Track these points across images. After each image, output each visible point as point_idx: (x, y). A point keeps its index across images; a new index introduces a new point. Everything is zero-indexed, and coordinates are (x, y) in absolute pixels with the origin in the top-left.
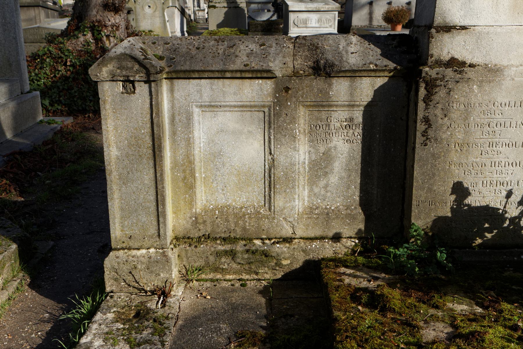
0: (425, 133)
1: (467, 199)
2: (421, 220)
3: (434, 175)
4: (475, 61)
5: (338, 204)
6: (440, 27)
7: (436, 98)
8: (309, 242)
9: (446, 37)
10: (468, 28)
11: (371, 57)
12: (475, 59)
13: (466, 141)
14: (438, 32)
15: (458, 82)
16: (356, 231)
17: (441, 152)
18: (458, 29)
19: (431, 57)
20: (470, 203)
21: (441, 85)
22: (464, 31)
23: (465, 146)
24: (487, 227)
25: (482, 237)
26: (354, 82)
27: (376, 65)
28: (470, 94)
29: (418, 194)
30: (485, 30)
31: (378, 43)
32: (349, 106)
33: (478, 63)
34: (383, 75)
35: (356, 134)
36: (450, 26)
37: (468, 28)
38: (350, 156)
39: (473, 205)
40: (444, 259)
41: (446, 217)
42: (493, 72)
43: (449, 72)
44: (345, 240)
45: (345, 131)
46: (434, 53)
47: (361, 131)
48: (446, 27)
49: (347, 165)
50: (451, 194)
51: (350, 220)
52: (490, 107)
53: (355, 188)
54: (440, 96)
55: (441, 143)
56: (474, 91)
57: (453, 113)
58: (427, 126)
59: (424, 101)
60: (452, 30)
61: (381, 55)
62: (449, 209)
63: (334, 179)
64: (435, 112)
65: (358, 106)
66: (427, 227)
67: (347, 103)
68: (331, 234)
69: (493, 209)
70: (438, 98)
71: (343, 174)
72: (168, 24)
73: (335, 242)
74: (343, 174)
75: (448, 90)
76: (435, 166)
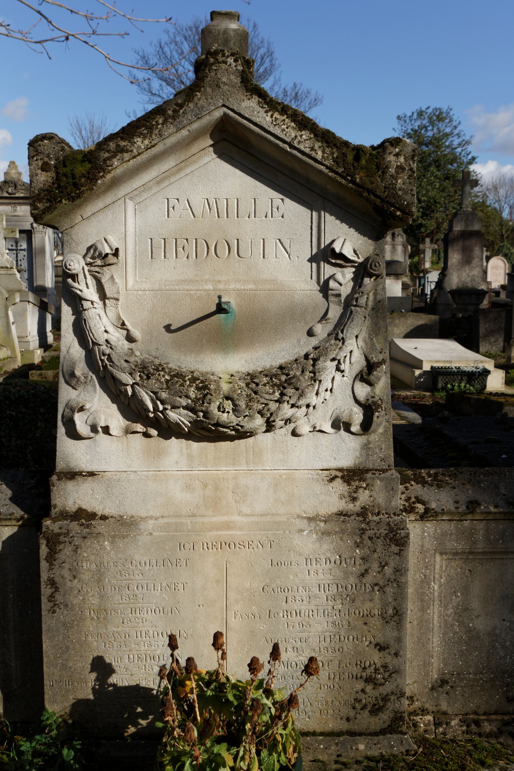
0: (51, 598)
1: (111, 678)
2: (56, 706)
3: (68, 648)
4: (107, 512)
6: (63, 473)
7: (61, 556)
9: (70, 486)
10: (96, 475)
13: (102, 607)
14: (59, 479)
15: (85, 538)
17: (73, 621)
19: (55, 508)
20: (115, 682)
21: (65, 542)
22: (90, 478)
23: (103, 613)
24: (139, 712)
25: (136, 724)
28: (99, 554)
29: (50, 672)
30: (115, 477)
33: (111, 515)
37: (96, 475)
39: (120, 684)
40: (72, 758)
42: (126, 526)
43: (74, 526)
46: (58, 503)
48: (70, 472)
50: (91, 671)
52: (127, 566)
55: (72, 609)
56: (105, 549)
58: (53, 590)
59: (47, 559)
60: (77, 477)
61: (10, 499)
62: (90, 691)
64: (62, 573)
66: (66, 713)
69: (145, 689)
70: (64, 557)
72: (13, 328)
75: (74, 548)
76: (69, 638)
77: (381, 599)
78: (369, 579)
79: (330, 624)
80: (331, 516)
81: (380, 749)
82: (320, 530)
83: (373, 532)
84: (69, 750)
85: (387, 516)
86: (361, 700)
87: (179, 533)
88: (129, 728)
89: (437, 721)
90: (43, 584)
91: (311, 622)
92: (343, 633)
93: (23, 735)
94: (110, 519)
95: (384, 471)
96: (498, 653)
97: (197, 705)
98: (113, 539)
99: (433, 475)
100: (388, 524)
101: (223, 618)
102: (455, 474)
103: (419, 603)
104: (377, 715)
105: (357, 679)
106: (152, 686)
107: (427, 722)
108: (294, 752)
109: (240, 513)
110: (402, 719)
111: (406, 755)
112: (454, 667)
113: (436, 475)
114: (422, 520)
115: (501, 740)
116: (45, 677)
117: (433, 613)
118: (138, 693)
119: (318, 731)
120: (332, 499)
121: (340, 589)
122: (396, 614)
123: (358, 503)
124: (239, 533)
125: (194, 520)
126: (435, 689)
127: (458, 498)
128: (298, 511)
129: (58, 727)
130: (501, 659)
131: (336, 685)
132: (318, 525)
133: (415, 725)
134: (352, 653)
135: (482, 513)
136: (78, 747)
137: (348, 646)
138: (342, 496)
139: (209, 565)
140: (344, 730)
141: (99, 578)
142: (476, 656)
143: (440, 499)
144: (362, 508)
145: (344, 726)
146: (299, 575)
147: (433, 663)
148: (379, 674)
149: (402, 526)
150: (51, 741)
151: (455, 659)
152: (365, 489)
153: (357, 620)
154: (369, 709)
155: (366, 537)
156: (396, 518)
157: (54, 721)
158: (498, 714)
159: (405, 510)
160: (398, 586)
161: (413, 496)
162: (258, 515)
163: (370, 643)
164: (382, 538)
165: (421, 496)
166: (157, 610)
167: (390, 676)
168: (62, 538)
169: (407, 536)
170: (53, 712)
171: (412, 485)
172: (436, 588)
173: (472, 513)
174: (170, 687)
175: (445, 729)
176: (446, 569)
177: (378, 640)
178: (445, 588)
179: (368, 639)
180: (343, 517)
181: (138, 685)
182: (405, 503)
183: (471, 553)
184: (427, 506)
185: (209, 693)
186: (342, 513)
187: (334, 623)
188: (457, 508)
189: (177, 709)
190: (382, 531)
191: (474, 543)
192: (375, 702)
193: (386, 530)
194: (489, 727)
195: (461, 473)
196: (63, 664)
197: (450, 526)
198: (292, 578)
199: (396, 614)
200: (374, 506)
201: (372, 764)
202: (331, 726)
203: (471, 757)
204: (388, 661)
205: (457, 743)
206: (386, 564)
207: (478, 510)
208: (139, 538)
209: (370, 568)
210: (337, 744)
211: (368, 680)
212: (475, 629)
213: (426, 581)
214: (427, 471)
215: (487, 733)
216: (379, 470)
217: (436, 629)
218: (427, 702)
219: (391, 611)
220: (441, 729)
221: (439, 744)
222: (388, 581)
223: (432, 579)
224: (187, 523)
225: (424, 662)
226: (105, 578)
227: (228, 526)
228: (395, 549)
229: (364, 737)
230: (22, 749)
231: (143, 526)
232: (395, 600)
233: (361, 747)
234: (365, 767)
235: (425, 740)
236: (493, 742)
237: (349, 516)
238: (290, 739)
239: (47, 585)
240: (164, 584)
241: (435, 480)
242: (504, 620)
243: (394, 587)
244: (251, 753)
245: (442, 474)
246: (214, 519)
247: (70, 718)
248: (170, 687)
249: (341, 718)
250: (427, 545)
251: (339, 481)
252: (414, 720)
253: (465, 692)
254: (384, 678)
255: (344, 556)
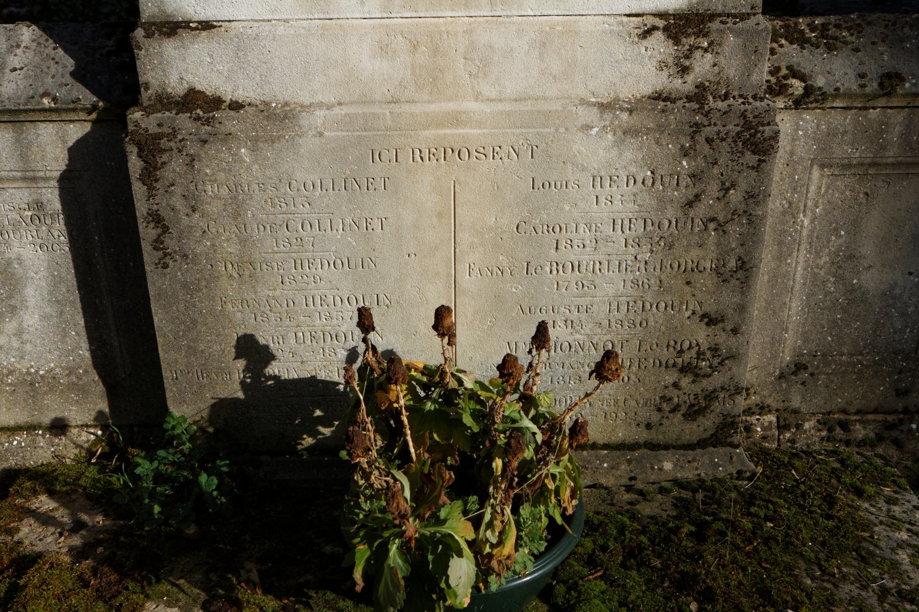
0: (158, 244)
1: (270, 366)
2: (186, 408)
4: (240, 95)
5: (52, 365)
6: (154, 24)
7: (167, 174)
8: (6, 436)
9: (169, 48)
10: (215, 27)
11: (49, 80)
12: (241, 92)
13: (246, 259)
14: (148, 36)
15: (205, 142)
16: (93, 413)
17: (199, 280)
18: (193, 29)
19: (147, 89)
22: (204, 33)
23: (247, 269)
24: (318, 417)
26: (23, 131)
27: (55, 99)
28: (230, 170)
30: (250, 31)
31: (75, 44)
32: (24, 179)
33: (248, 100)
34: (76, 118)
35: (56, 234)
36: (178, 22)
37: (215, 27)
38: (53, 276)
39: (285, 376)
40: (214, 487)
41: (234, 399)
42: (275, 120)
43: (184, 121)
44: (75, 431)
45: (31, 229)
47: (64, 228)
49: (51, 293)
50: (236, 358)
51: (77, 395)
53: (77, 334)
54: (174, 171)
57: (207, 203)
58: (159, 231)
59: (141, 179)
60: (180, 31)
62: (237, 386)
63: (31, 319)
65: (46, 179)
66: (202, 417)
67: (19, 174)
68: (47, 420)
69: (326, 383)
70: (171, 175)
71: (48, 310)
73: (56, 435)
74: (48, 310)
75: (188, 159)
76: (194, 306)
77: (718, 244)
78: (701, 211)
79: (629, 284)
80: (640, 100)
81: (697, 469)
82: (620, 127)
83: (715, 129)
84: (209, 476)
85: (741, 100)
86: (671, 399)
87: (371, 133)
88: (304, 439)
89: (782, 423)
90: (140, 221)
91: (597, 282)
92: (649, 298)
93: (141, 447)
94: (247, 108)
95: (743, 17)
96: (892, 324)
97: (409, 432)
98: (254, 144)
99: (820, 28)
100: (743, 115)
101: (449, 275)
102: (859, 25)
103: (776, 247)
104: (695, 420)
105: (667, 367)
106: (336, 378)
107: (766, 424)
108: (573, 497)
109: (478, 97)
110: (733, 425)
111: (737, 479)
112: (818, 345)
113: (825, 26)
114: (796, 109)
115: (880, 450)
116: (163, 365)
117: (797, 262)
118: (314, 389)
119: (601, 442)
120: (644, 69)
121: (650, 228)
122: (741, 268)
123: (690, 78)
124: (476, 131)
125: (396, 108)
126: (785, 377)
127: (864, 69)
128: (582, 92)
129: (192, 439)
130: (895, 333)
131: (633, 377)
132: (617, 117)
133: (748, 429)
134: (663, 328)
135: (906, 95)
136: (225, 469)
137: (656, 318)
138: (662, 65)
139: (424, 187)
140: (642, 441)
141: (236, 208)
142: (856, 329)
143: (832, 70)
144: (697, 87)
145: (643, 435)
146: (579, 203)
147: (786, 340)
148: (703, 360)
149: (766, 118)
150: (182, 459)
151: (821, 333)
152: (706, 50)
153: (675, 277)
154: (682, 412)
155: (701, 139)
156: (758, 104)
157: (186, 430)
158: (878, 413)
159: (770, 90)
160: (750, 222)
161: (783, 65)
162: (510, 100)
163: (694, 313)
164: (729, 140)
165: (799, 65)
166: (339, 261)
167: (721, 363)
168: (164, 143)
169: (776, 136)
170: (183, 416)
171: (781, 46)
172: (806, 223)
173: (888, 94)
174: (362, 398)
175: (794, 434)
176: (826, 191)
177: (706, 309)
178: (820, 223)
179: (691, 307)
180: (662, 103)
181: (313, 377)
182: (770, 78)
183: (873, 165)
184: (809, 82)
185: (429, 406)
186: (660, 95)
187: (635, 282)
188: (862, 86)
189: (375, 431)
190: (731, 127)
191: (883, 148)
192: (693, 402)
193: (738, 125)
194: (863, 432)
195: (869, 24)
196: (189, 347)
197: (845, 119)
198: (567, 208)
199: (741, 268)
200: (719, 83)
201: (685, 494)
202: (620, 435)
203: (839, 481)
204: (721, 340)
205: (814, 457)
206: (733, 186)
207: (900, 91)
208: (300, 141)
209: (704, 191)
210: (629, 462)
211: (685, 370)
212: (861, 287)
213: (791, 211)
214: (808, 20)
215: (858, 440)
216: (734, 16)
217: (797, 287)
218: (770, 396)
219: (732, 263)
220: (788, 435)
221: (786, 460)
222: (733, 214)
223: (802, 208)
224: (384, 114)
225: (773, 338)
226: (246, 211)
227: (456, 119)
228: (750, 158)
229: (671, 451)
230: (138, 471)
231: (305, 120)
232: (742, 245)
233: (668, 466)
234: (676, 498)
235: (765, 452)
236: (869, 454)
237: (673, 101)
238: (567, 478)
239: (148, 222)
240: (348, 220)
241: (823, 37)
242: (910, 274)
243: (743, 224)
244: (503, 515)
245: (836, 26)
246: (432, 107)
247: (210, 425)
248: (362, 398)
249: (638, 425)
250: (800, 151)
251: (659, 35)
252: (747, 421)
253: (832, 382)
254: (710, 367)
255: (660, 172)
